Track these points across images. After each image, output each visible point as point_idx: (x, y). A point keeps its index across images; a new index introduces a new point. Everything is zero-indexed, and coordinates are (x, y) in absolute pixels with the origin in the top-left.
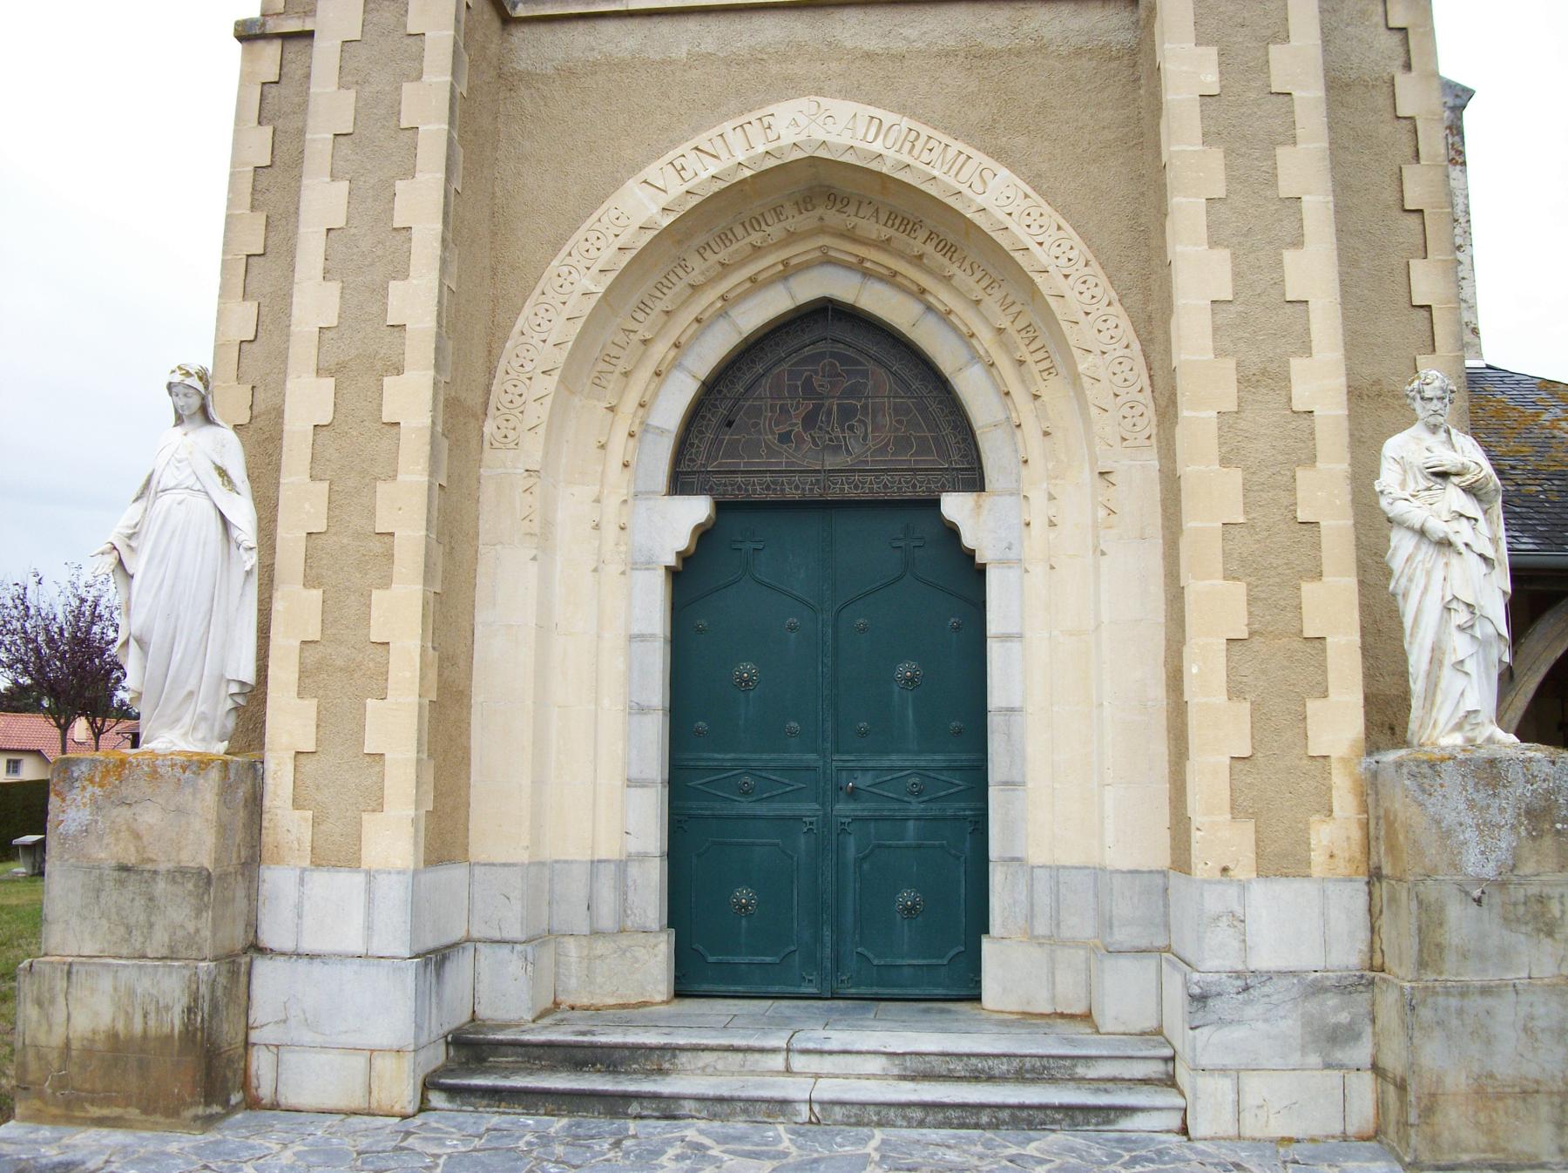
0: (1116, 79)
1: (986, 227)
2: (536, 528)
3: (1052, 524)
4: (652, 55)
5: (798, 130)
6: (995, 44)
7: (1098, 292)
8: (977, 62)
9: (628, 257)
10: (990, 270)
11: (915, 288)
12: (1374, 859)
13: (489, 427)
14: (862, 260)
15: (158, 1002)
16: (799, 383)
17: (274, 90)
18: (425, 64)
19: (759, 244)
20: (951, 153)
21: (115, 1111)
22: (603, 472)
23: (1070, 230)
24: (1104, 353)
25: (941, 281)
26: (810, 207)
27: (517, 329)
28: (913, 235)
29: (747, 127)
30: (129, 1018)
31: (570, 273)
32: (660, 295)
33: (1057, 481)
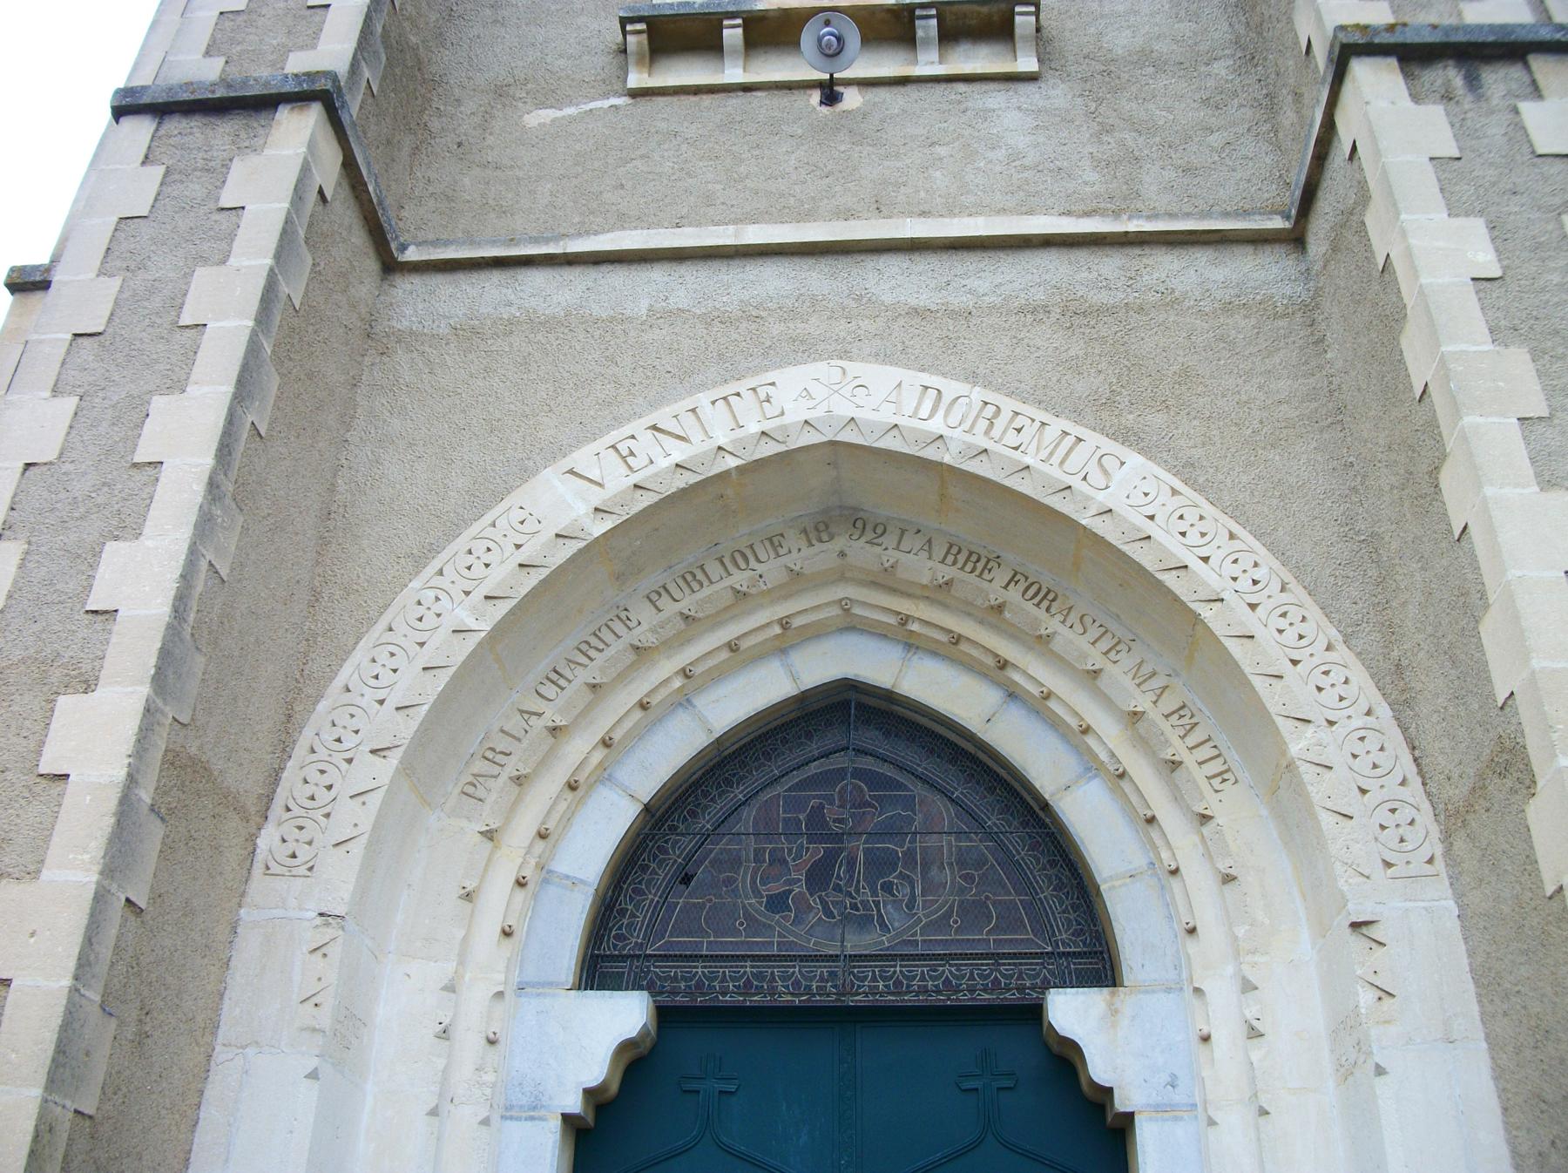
0: (1290, 340)
1: (1113, 538)
2: (325, 1018)
3: (1254, 1033)
4: (596, 311)
5: (811, 404)
6: (1103, 297)
7: (1307, 629)
8: (1077, 321)
9: (533, 579)
10: (1112, 625)
11: (990, 661)
13: (268, 839)
14: (905, 620)
18: (235, 244)
19: (744, 589)
20: (1052, 433)
22: (465, 939)
23: (1250, 539)
24: (1331, 723)
25: (1031, 648)
26: (825, 537)
27: (339, 682)
28: (986, 575)
31: (437, 599)
32: (584, 660)
33: (1257, 958)
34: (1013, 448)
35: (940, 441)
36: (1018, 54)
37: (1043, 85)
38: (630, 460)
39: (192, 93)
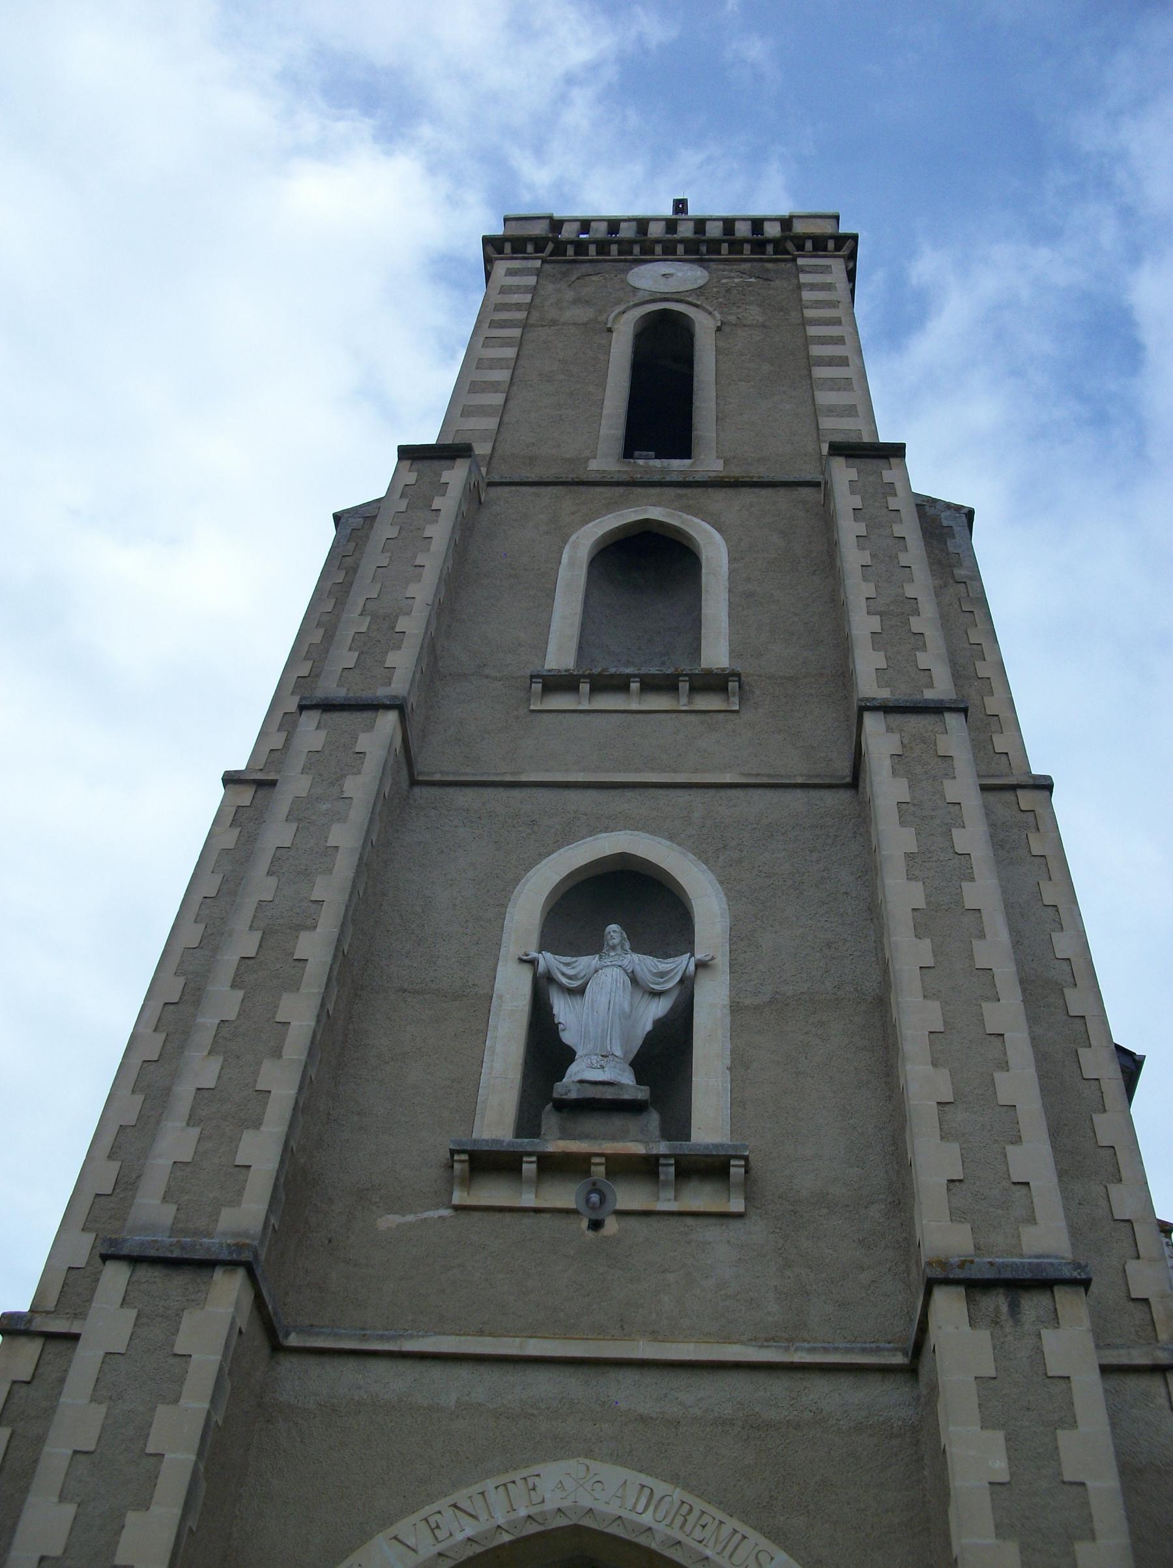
17: (23, 1391)
18: (185, 1388)
20: (726, 1531)
29: (510, 1486)
34: (698, 1541)
35: (649, 1532)
36: (731, 1196)
37: (747, 1222)
38: (436, 1531)
39: (157, 1250)
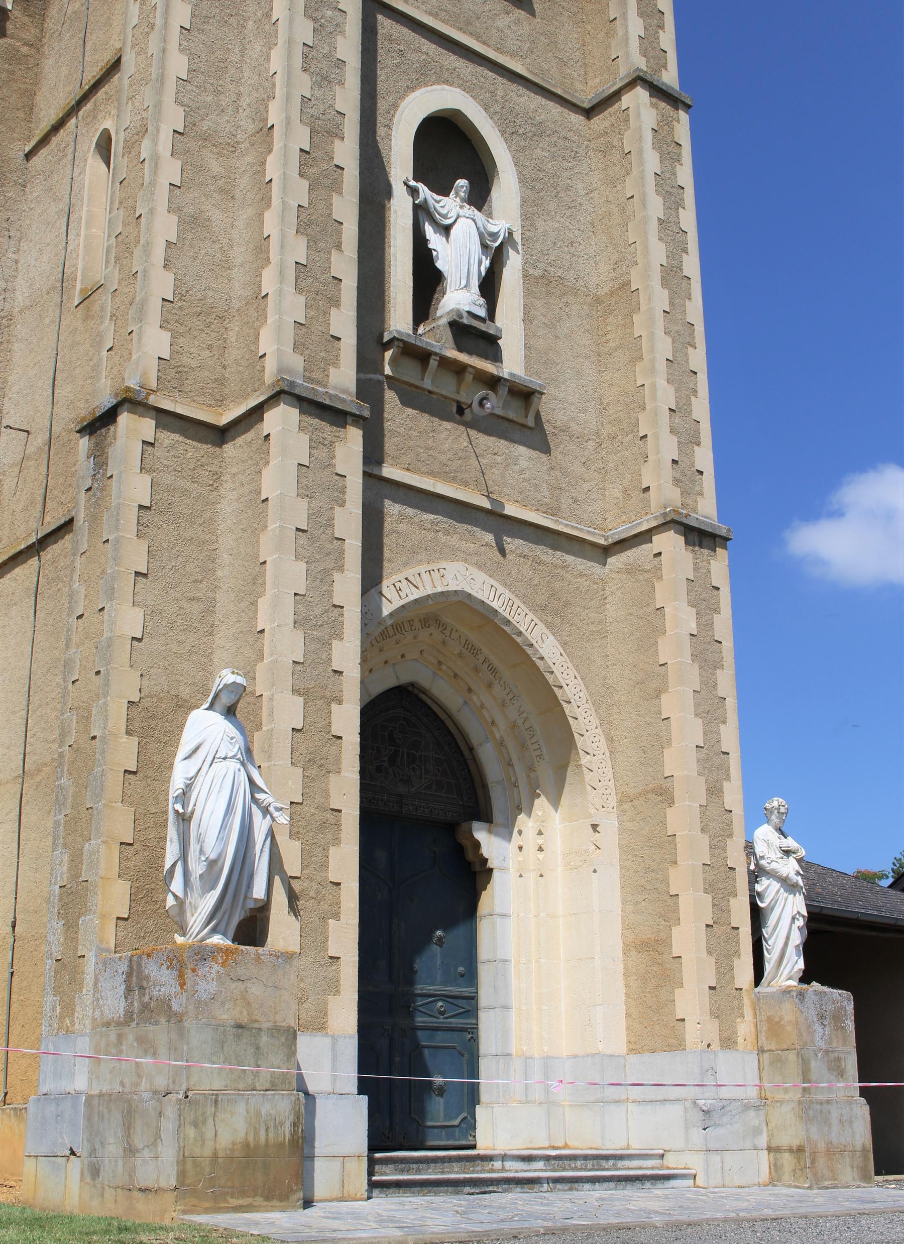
12: (760, 1042)
15: (275, 1119)
16: (386, 734)
21: (247, 1201)
30: (256, 1133)
